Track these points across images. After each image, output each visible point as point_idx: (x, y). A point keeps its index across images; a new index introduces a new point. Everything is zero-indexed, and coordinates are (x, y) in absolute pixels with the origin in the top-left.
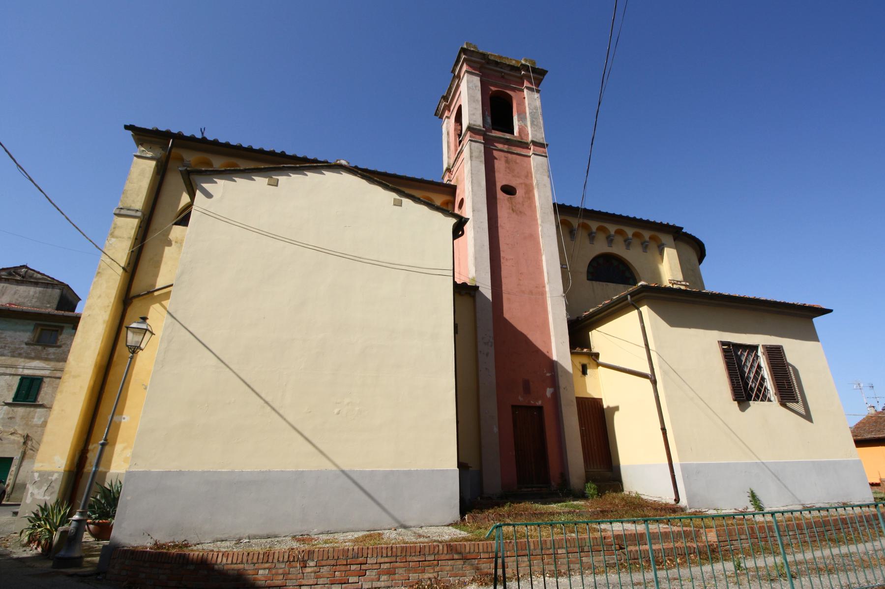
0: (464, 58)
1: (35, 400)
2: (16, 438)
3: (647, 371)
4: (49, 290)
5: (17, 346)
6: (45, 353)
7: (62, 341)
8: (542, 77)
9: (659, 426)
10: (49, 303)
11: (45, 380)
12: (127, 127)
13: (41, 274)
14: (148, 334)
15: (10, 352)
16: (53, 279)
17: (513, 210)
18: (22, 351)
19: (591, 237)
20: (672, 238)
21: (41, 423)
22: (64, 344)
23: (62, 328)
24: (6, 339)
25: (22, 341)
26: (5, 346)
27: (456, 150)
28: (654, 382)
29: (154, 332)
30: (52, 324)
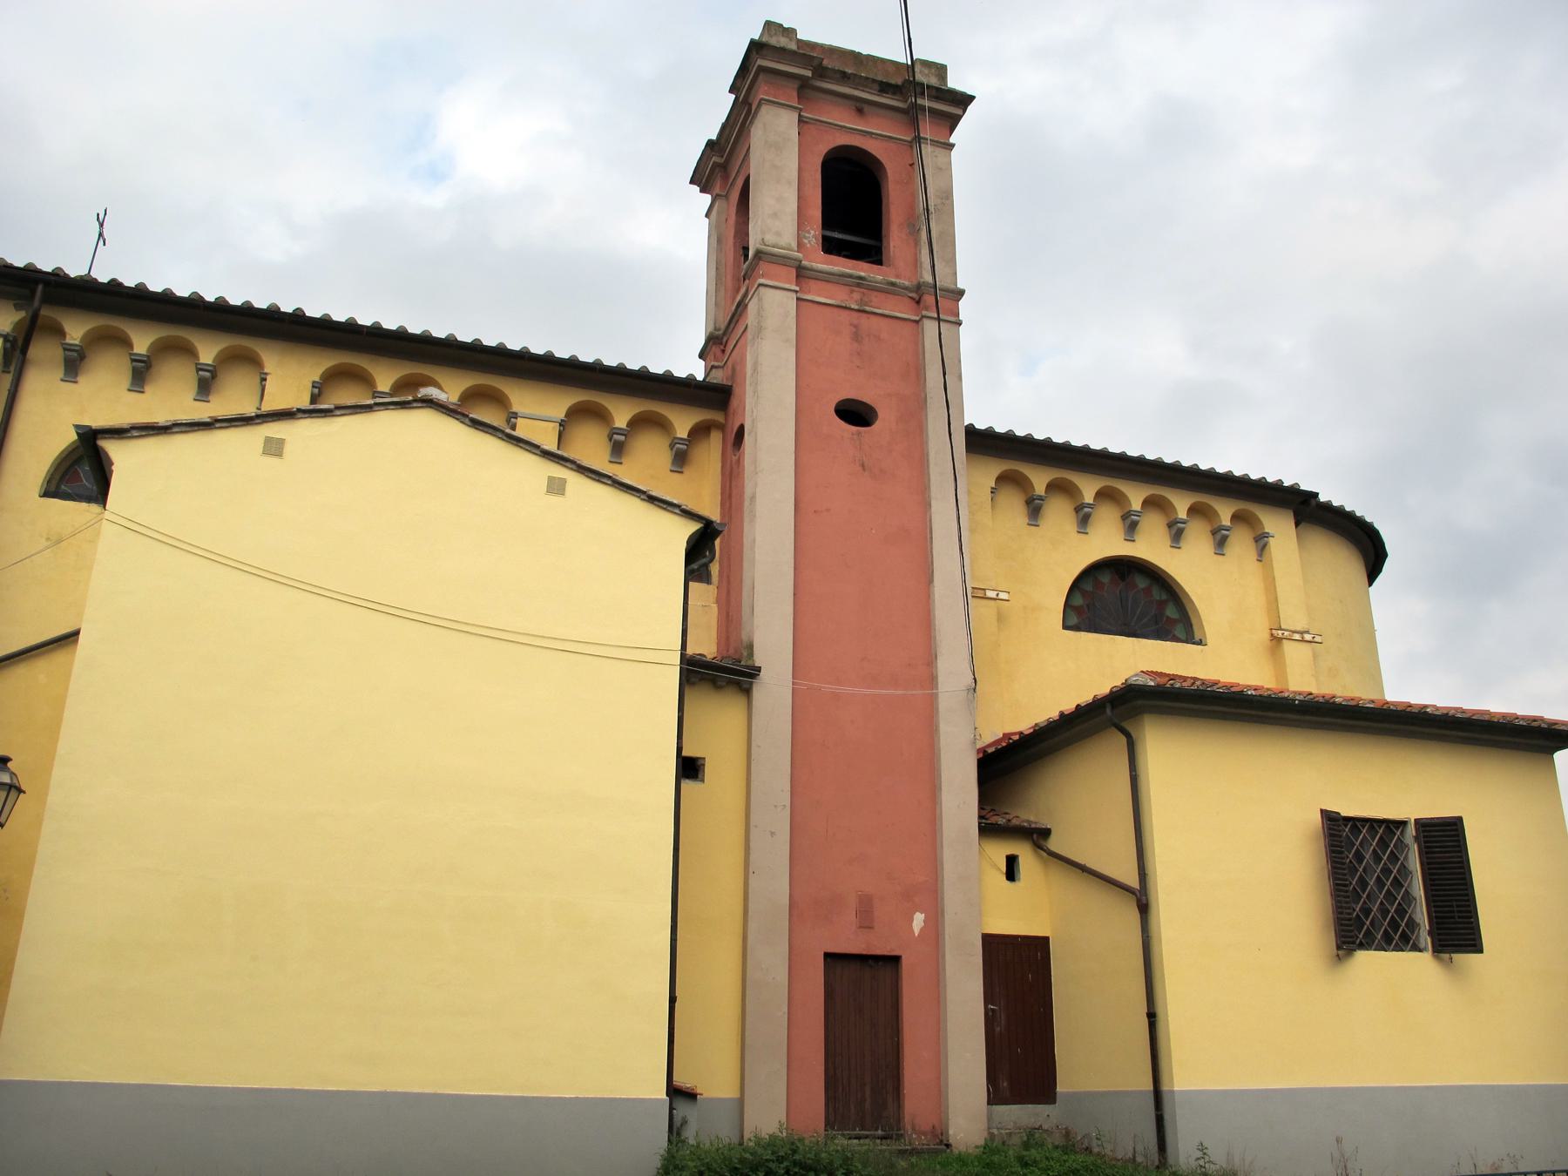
0: (714, 162)
8: (959, 112)
14: (13, 793)
19: (1084, 519)
20: (1292, 514)
27: (734, 299)
28: (1144, 908)
29: (23, 788)
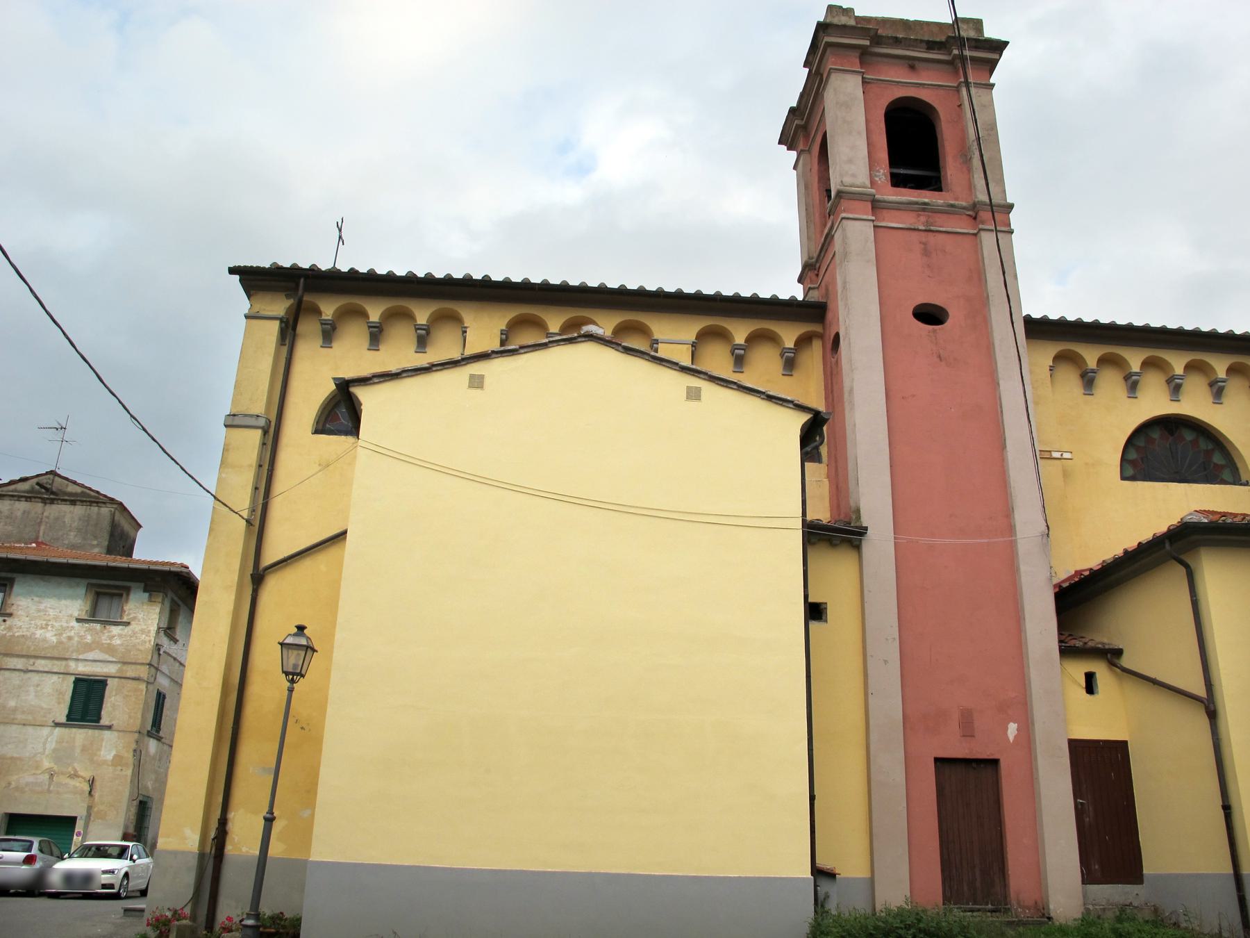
1: (98, 719)
2: (78, 784)
3: (1201, 691)
4: (95, 509)
5: (65, 625)
6: (106, 634)
7: (129, 614)
9: (1219, 802)
10: (96, 537)
11: (110, 681)
12: (232, 271)
13: (78, 485)
14: (309, 652)
15: (56, 635)
16: (98, 492)
17: (939, 357)
18: (72, 634)
21: (111, 758)
22: (134, 618)
23: (128, 590)
24: (46, 611)
25: (71, 616)
26: (47, 625)
27: (823, 231)
28: (1212, 714)
29: (316, 648)
30: (111, 583)
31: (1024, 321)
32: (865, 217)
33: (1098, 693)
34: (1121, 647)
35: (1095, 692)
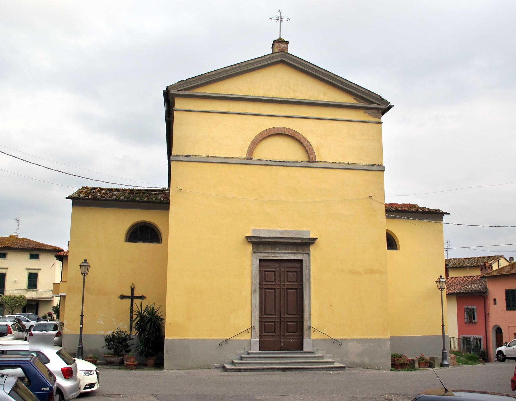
14: (89, 267)
31: (163, 366)
32: (268, 324)
33: (399, 250)
34: (8, 259)
35: (398, 249)
